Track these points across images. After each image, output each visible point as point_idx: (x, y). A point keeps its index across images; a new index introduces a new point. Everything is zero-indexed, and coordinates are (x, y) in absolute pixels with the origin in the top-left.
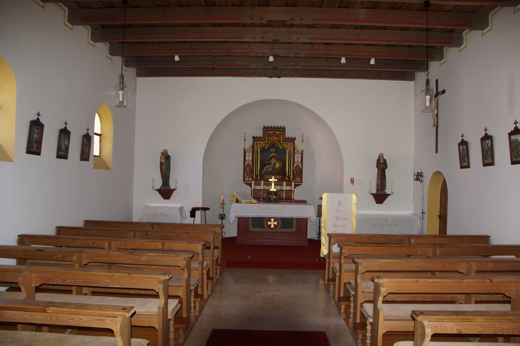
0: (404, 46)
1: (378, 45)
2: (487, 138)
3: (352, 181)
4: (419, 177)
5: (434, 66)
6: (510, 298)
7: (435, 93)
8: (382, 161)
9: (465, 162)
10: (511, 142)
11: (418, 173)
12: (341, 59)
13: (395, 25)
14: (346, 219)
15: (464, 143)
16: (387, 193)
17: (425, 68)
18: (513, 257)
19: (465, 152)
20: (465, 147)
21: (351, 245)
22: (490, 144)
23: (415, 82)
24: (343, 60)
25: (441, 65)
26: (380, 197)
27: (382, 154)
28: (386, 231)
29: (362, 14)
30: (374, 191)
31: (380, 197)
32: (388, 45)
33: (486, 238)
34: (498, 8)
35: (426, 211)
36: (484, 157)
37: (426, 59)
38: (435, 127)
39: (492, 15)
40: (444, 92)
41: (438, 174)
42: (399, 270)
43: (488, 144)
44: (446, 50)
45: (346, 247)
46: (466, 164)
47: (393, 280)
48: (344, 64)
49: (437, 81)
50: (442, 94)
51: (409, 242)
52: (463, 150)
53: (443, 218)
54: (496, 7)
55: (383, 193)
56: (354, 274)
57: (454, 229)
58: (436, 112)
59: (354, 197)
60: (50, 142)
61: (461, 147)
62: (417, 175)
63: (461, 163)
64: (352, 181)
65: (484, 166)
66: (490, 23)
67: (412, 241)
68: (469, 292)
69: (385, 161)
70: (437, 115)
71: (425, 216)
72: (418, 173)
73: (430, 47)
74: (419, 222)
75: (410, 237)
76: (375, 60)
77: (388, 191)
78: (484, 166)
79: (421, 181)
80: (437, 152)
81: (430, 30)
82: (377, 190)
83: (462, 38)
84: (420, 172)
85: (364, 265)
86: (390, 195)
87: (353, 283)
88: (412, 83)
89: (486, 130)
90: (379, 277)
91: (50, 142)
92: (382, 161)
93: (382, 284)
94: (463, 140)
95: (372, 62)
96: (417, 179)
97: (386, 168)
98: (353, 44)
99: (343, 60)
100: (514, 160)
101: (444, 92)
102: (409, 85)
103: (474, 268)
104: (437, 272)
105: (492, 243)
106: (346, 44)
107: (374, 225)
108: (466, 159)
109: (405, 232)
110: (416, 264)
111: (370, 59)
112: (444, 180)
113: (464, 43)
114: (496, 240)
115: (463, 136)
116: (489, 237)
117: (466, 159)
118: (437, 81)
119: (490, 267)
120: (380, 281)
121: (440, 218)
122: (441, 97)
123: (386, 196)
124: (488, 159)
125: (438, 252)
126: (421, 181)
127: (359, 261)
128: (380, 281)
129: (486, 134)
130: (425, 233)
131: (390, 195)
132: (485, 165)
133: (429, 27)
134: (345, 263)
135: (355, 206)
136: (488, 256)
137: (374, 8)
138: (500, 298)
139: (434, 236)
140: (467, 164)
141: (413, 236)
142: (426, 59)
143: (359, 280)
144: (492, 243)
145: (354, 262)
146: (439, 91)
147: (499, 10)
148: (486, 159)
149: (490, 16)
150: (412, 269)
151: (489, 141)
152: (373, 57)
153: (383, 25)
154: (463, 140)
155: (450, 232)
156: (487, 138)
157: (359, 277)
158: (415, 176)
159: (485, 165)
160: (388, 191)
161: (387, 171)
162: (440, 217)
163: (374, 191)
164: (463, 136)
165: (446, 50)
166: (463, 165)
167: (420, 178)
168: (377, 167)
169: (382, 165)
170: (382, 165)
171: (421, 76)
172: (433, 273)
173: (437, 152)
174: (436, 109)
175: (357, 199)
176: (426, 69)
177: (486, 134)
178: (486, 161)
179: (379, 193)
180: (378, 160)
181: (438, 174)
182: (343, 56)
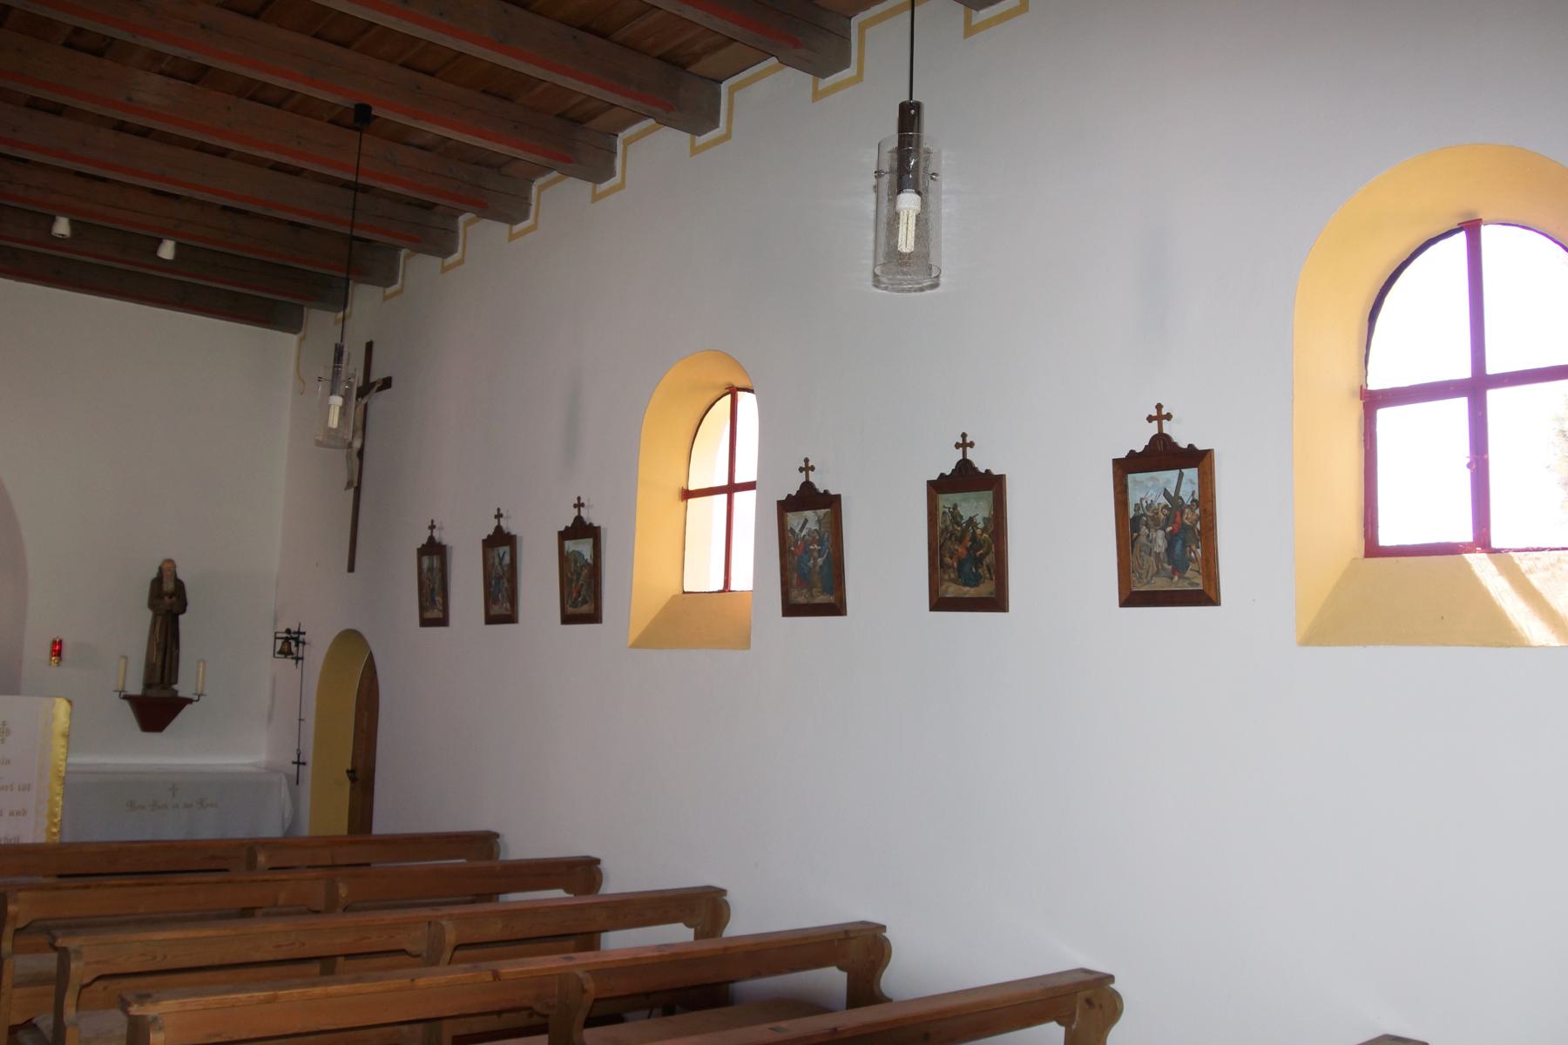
0: (279, 221)
1: (190, 200)
2: (500, 541)
3: (57, 649)
4: (290, 644)
5: (364, 298)
6: (546, 1016)
7: (358, 381)
8: (169, 586)
9: (434, 607)
10: (563, 558)
11: (288, 631)
12: (52, 220)
13: (258, 153)
14: (26, 788)
15: (434, 550)
16: (181, 694)
17: (338, 300)
18: (558, 894)
19: (437, 577)
20: (436, 563)
21: (41, 888)
22: (507, 559)
23: (302, 339)
24: (62, 227)
25: (386, 298)
26: (156, 708)
27: (170, 561)
28: (171, 828)
29: (151, 90)
30: (136, 688)
31: (156, 708)
32: (225, 208)
33: (486, 842)
34: (555, 174)
35: (308, 757)
36: (490, 597)
37: (344, 275)
38: (351, 491)
39: (542, 188)
40: (387, 383)
41: (351, 639)
42: (217, 961)
43: (501, 559)
44: (407, 257)
45: (22, 895)
46: (436, 613)
47: (193, 1003)
48: (62, 239)
49: (369, 346)
50: (379, 389)
51: (252, 864)
52: (431, 569)
53: (362, 778)
54: (550, 169)
55: (166, 694)
56: (52, 988)
57: (392, 815)
58: (357, 444)
59: (62, 708)
60: (1062, 538)
61: (426, 560)
62: (287, 640)
63: (422, 609)
64: (57, 649)
65: (1125, 602)
66: (533, 209)
67: (261, 858)
68: (434, 1015)
69: (180, 586)
70: (361, 453)
71: (307, 772)
72: (288, 631)
73: (358, 239)
74: (285, 792)
75: (250, 848)
76: (178, 247)
77: (183, 688)
78: (1125, 602)
79: (297, 659)
80: (351, 569)
81: (366, 189)
82: (148, 685)
83: (455, 232)
84: (294, 628)
85: (89, 955)
86: (190, 701)
87: (46, 1022)
88: (293, 339)
89: (499, 516)
90: (143, 998)
91: (1062, 538)
92: (169, 586)
93: (155, 1019)
94: (431, 538)
95: (167, 251)
96: (285, 652)
97: (184, 611)
98: (105, 180)
99: (62, 227)
100: (570, 610)
101: (387, 383)
102: (286, 342)
103: (451, 937)
104: (341, 960)
105: (502, 857)
106: (79, 174)
107: (132, 805)
108: (438, 599)
109: (239, 830)
110: (270, 936)
111: (159, 241)
112: (371, 657)
113: (460, 248)
114: (520, 846)
115: (432, 527)
116: (497, 835)
117: (438, 599)
118: (369, 346)
119: (495, 930)
120: (149, 1010)
121: (353, 780)
122: (378, 401)
123: (177, 705)
124: (502, 604)
125: (343, 891)
126: (297, 659)
127: (71, 943)
128: (149, 1010)
129: (499, 529)
130: (305, 831)
131: (190, 701)
132: (491, 619)
133: (362, 180)
134: (16, 950)
135: (63, 742)
136: (490, 897)
137: (193, 82)
138: (521, 1020)
139: (333, 842)
140: (440, 615)
141: (267, 844)
142: (344, 275)
143: (70, 1013)
144: (502, 857)
145: (56, 949)
146: (373, 379)
147: (555, 181)
148: (496, 601)
149: (534, 190)
150: (257, 957)
151: (507, 548)
152: (170, 234)
153: (218, 142)
154: (431, 538)
155: (385, 822)
156: (500, 541)
157: (70, 999)
158: (279, 643)
159: (491, 619)
160: (183, 688)
161: (182, 618)
162: (352, 773)
163: (136, 688)
164: (432, 527)
165: (407, 257)
166: (428, 615)
167: (294, 649)
168: (152, 605)
169: (168, 600)
170: (168, 600)
171: (320, 321)
172: (327, 964)
173: (351, 569)
174: (360, 433)
175: (71, 716)
176: (343, 303)
177: (499, 529)
178: (496, 610)
179: (154, 693)
180: (157, 583)
181: (351, 639)
182: (65, 211)
